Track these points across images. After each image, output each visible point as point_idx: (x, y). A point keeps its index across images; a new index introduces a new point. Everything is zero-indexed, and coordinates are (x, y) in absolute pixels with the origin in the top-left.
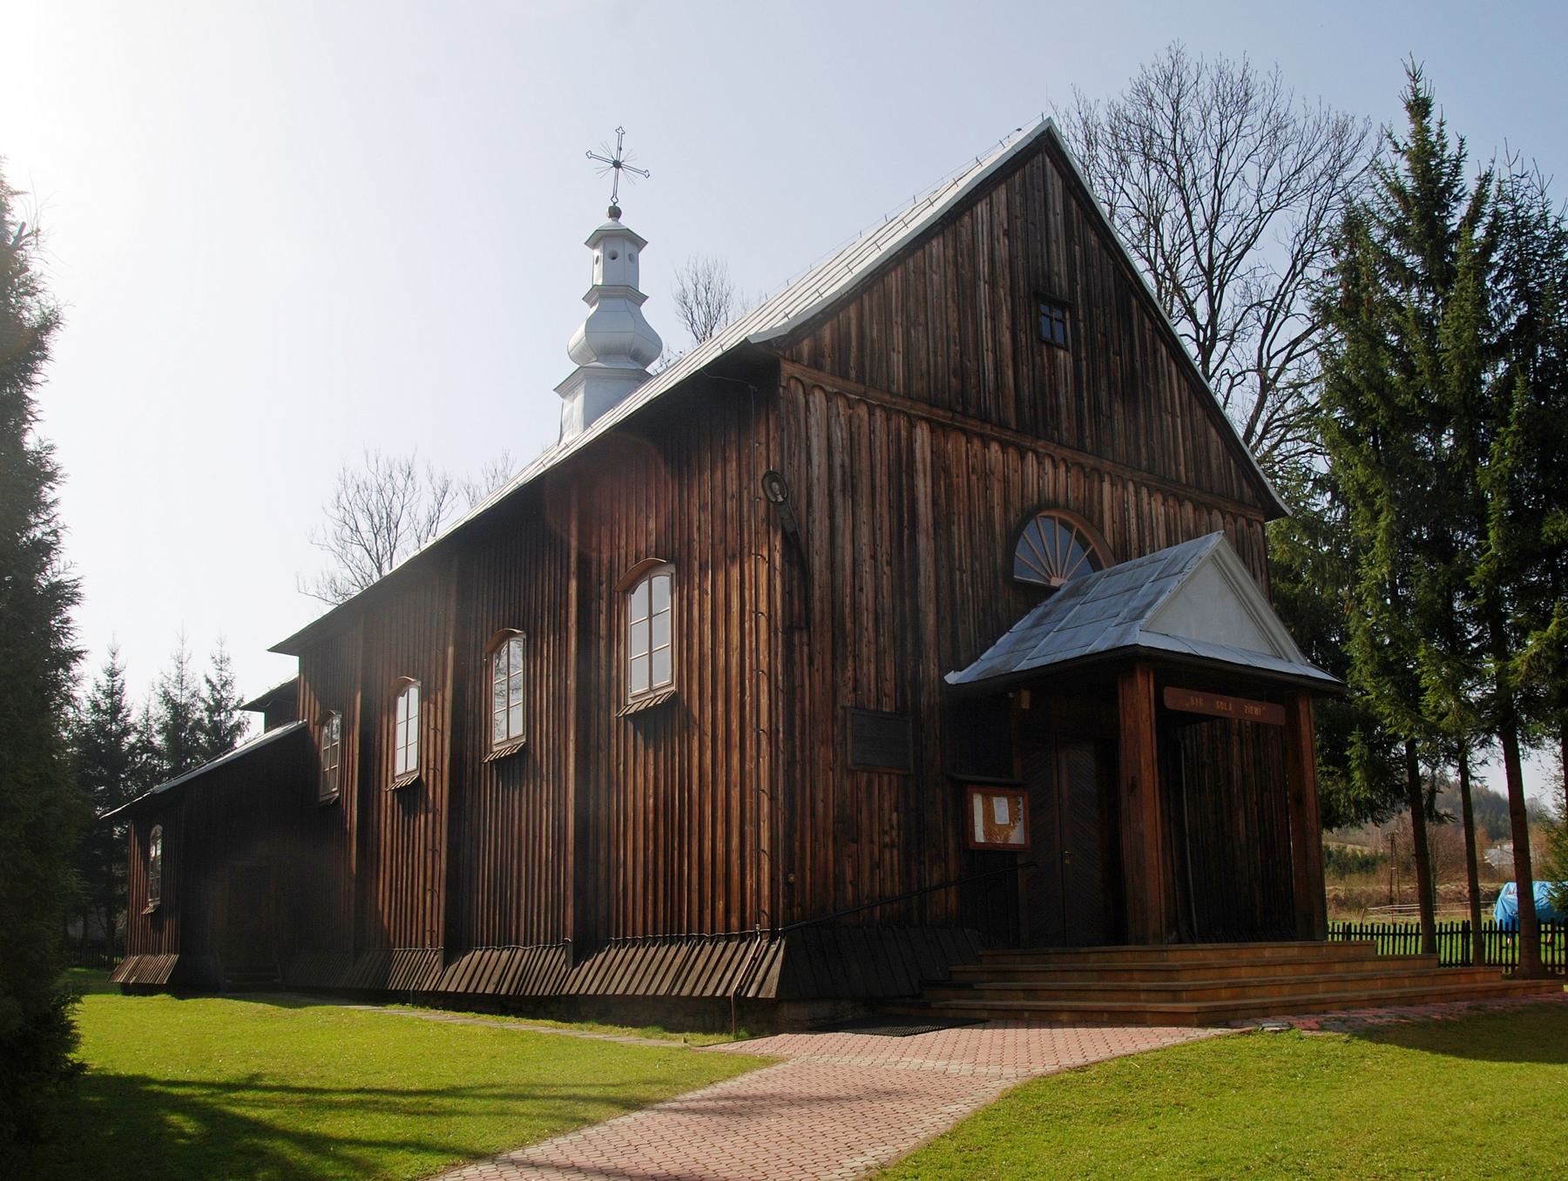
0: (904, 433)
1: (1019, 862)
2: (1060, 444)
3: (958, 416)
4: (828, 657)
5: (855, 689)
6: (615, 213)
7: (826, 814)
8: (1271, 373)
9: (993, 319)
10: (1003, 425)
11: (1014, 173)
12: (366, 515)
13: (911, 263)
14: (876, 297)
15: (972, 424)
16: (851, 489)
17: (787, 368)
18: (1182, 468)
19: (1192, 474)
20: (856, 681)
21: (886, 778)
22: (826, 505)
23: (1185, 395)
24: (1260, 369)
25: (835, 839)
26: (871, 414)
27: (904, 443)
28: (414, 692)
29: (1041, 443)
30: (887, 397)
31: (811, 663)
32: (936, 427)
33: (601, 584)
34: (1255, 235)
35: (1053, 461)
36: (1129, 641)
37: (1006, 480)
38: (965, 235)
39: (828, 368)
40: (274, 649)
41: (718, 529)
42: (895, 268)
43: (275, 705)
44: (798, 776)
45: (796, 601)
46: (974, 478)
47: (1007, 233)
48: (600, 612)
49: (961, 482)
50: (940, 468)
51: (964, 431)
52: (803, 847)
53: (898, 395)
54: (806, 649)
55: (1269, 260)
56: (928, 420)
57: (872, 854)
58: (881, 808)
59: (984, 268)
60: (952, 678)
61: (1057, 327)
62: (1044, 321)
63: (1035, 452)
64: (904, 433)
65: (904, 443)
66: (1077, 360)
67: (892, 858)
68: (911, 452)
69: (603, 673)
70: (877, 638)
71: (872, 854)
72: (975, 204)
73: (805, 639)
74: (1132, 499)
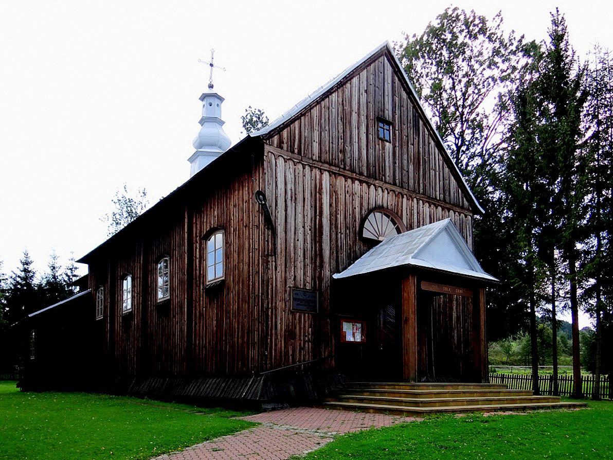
0: (318, 177)
2: (386, 182)
3: (341, 170)
5: (295, 279)
6: (211, 87)
10: (361, 174)
11: (370, 65)
14: (307, 118)
15: (349, 174)
18: (438, 193)
19: (442, 196)
20: (295, 277)
23: (441, 162)
26: (304, 168)
28: (129, 279)
29: (377, 181)
30: (311, 161)
32: (331, 173)
35: (382, 190)
37: (362, 197)
42: (316, 106)
43: (83, 282)
46: (347, 195)
47: (366, 91)
49: (342, 197)
50: (333, 192)
51: (344, 176)
53: (316, 160)
54: (274, 263)
56: (329, 171)
57: (300, 344)
58: (304, 327)
59: (355, 108)
60: (336, 276)
62: (381, 130)
63: (374, 185)
64: (318, 177)
66: (394, 147)
69: (198, 272)
71: (300, 344)
72: (352, 78)
73: (274, 260)
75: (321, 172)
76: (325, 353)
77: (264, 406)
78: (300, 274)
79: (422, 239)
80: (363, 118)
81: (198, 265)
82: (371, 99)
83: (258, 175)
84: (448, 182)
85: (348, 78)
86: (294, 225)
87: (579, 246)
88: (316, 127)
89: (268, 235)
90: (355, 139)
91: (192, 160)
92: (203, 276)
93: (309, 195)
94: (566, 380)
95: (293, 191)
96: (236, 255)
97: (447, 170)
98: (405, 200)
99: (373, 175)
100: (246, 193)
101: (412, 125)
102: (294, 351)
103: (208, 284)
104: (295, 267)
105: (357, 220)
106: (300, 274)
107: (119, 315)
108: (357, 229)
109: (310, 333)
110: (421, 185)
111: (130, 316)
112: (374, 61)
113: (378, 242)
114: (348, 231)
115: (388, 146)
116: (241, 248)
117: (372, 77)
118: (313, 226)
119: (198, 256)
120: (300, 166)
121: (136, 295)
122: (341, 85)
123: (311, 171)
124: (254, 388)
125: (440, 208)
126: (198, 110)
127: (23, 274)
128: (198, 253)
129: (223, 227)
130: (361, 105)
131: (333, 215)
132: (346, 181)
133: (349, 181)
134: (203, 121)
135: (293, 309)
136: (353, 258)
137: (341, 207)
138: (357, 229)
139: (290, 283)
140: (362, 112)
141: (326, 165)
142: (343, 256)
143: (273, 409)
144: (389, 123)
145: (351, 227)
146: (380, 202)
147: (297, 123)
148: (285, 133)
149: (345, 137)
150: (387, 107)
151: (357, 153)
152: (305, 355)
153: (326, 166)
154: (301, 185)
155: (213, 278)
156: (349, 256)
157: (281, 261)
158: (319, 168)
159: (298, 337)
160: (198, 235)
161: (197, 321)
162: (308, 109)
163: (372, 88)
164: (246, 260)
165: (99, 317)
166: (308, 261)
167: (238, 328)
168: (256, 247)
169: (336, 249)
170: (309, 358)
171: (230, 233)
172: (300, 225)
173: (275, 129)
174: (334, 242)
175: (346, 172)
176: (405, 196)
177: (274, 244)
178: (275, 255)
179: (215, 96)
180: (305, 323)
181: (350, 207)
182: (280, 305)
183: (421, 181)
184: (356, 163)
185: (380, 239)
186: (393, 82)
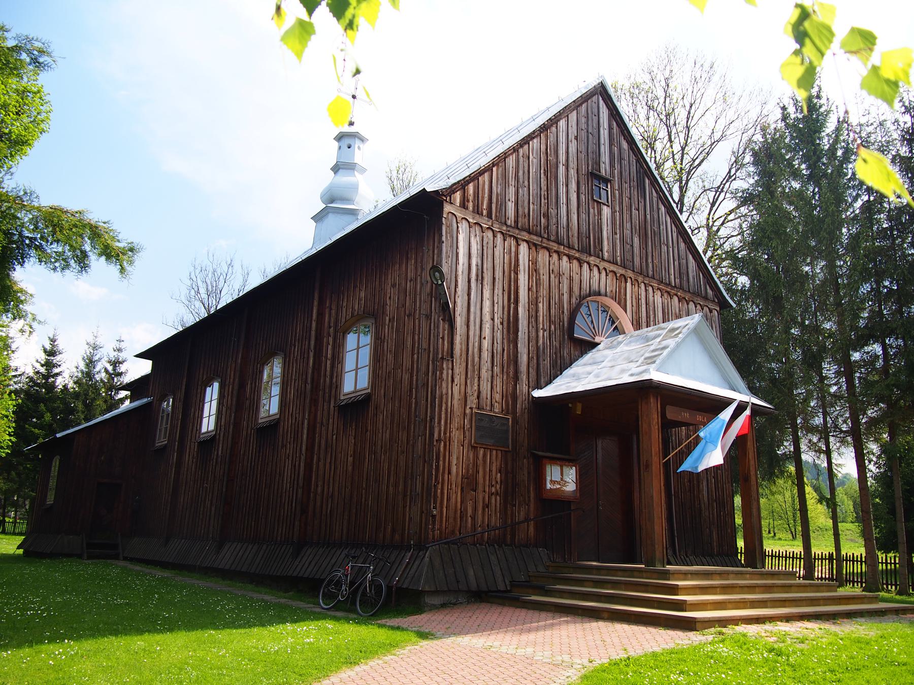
0: (513, 249)
1: (572, 508)
2: (603, 259)
3: (544, 240)
4: (463, 377)
5: (478, 397)
7: (457, 472)
8: (715, 229)
9: (567, 186)
10: (570, 247)
11: (581, 105)
12: (205, 285)
13: (521, 151)
14: (500, 169)
15: (555, 246)
16: (481, 278)
17: (447, 208)
18: (672, 277)
19: (678, 281)
20: (479, 392)
21: (494, 452)
22: (466, 288)
23: (675, 235)
24: (709, 228)
25: (462, 488)
26: (494, 236)
27: (513, 254)
28: (216, 385)
29: (592, 258)
30: (505, 228)
31: (453, 381)
32: (531, 245)
33: (330, 327)
34: (708, 154)
35: (599, 269)
36: (646, 377)
37: (571, 279)
38: (552, 138)
39: (471, 208)
40: (755, 6)
41: (402, 298)
42: (512, 154)
43: (137, 387)
44: (442, 449)
45: (446, 342)
46: (552, 276)
47: (576, 138)
48: (328, 344)
49: (545, 278)
50: (534, 270)
51: (548, 249)
52: (442, 493)
53: (510, 226)
54: (450, 371)
55: (716, 166)
56: (527, 242)
57: (484, 498)
58: (490, 471)
59: (562, 157)
60: (537, 393)
61: (603, 193)
63: (588, 263)
64: (513, 249)
65: (513, 254)
66: (613, 212)
67: (496, 501)
68: (517, 260)
69: (328, 380)
70: (492, 367)
71: (484, 498)
72: (559, 121)
73: (450, 366)
74: (643, 294)
75: (517, 242)
76: (519, 513)
77: (429, 600)
78: (486, 387)
79: (664, 343)
80: (572, 172)
81: (328, 369)
82: (583, 148)
83: (431, 243)
84: (684, 261)
85: (553, 121)
86: (477, 315)
87: (856, 356)
88: (512, 182)
89: (444, 330)
90: (563, 199)
91: (318, 218)
92: (337, 385)
93: (501, 274)
94: (853, 561)
95: (480, 267)
96: (390, 357)
97: (682, 245)
98: (629, 285)
99: (587, 247)
100: (411, 267)
101: (635, 183)
102: (475, 509)
103: (342, 398)
104: (479, 378)
105: (565, 311)
106: (486, 387)
107: (193, 440)
108: (566, 325)
109: (499, 480)
110: (650, 265)
111: (210, 441)
112: (587, 101)
113: (594, 345)
114: (553, 327)
115: (606, 211)
116: (400, 345)
117: (584, 120)
118: (505, 319)
119: (329, 356)
120: (490, 234)
121: (224, 409)
122: (544, 128)
123: (505, 240)
124: (415, 567)
125: (676, 299)
126: (331, 152)
127: (43, 370)
128: (330, 352)
129: (373, 315)
130: (570, 155)
131: (533, 303)
132: (550, 256)
133: (555, 256)
134: (336, 169)
135: (475, 443)
136: (560, 367)
137: (543, 292)
138: (566, 325)
139: (472, 401)
140: (571, 165)
141: (524, 233)
142: (546, 363)
143: (443, 606)
144: (606, 181)
145: (557, 321)
146: (595, 287)
147: (486, 175)
148: (471, 188)
149: (550, 195)
150: (603, 159)
151: (565, 218)
152: (490, 516)
153: (526, 236)
154: (490, 259)
155: (353, 389)
156: (554, 364)
157: (459, 369)
158: (515, 237)
159: (480, 487)
160: (332, 325)
161: (322, 456)
162: (501, 159)
163: (583, 134)
164: (407, 363)
165: (161, 441)
166: (497, 369)
167: (389, 468)
168: (425, 346)
169: (536, 355)
170: (496, 521)
171: (383, 325)
172: (487, 317)
173: (458, 182)
174: (533, 339)
175: (551, 243)
176: (629, 280)
177: (452, 343)
178: (452, 357)
179: (354, 135)
180: (491, 465)
181: (555, 292)
182: (456, 435)
183: (650, 260)
184: (563, 232)
185: (597, 339)
186: (610, 128)
